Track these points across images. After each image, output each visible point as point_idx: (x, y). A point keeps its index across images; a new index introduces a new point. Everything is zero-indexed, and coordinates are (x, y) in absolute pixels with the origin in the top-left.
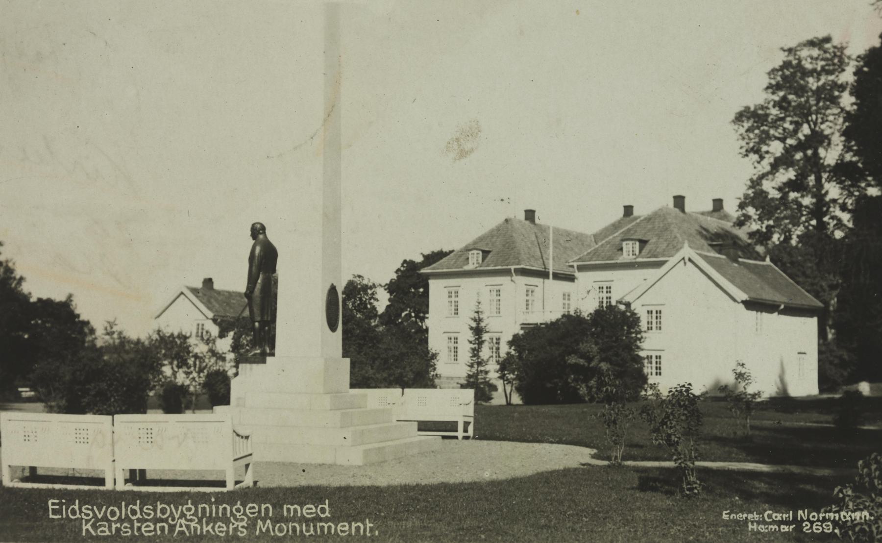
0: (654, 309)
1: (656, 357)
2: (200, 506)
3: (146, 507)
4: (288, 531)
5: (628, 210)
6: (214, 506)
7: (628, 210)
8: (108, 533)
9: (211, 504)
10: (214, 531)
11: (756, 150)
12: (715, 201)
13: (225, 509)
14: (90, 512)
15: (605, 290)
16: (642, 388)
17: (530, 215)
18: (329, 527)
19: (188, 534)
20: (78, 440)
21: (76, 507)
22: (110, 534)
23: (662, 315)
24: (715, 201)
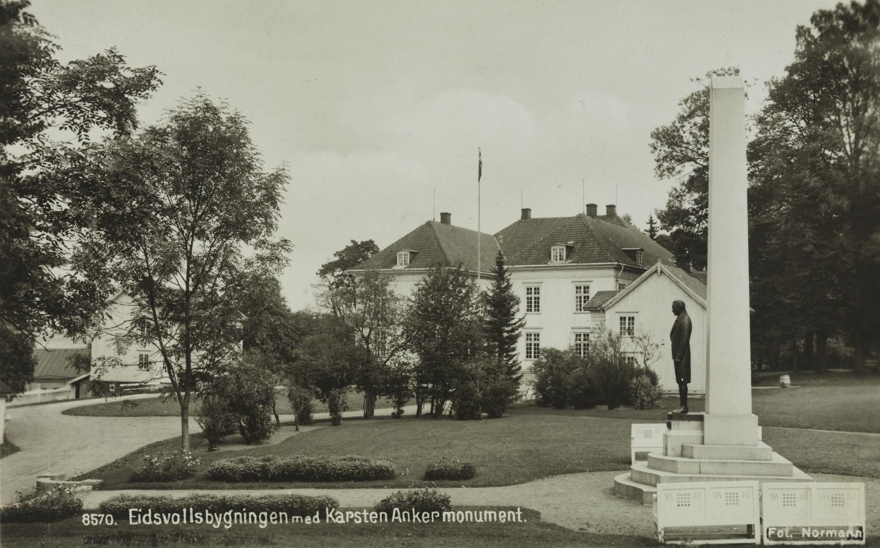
0: (627, 316)
1: (629, 318)
2: (433, 513)
3: (285, 514)
4: (223, 517)
5: (526, 212)
6: (245, 514)
7: (526, 212)
8: (342, 521)
9: (242, 513)
10: (421, 519)
11: (154, 88)
12: (608, 207)
13: (469, 514)
14: (360, 518)
15: (533, 291)
16: (202, 340)
17: (445, 217)
18: (493, 515)
19: (400, 521)
20: (687, 496)
21: (150, 515)
22: (482, 521)
23: (540, 300)
24: (608, 207)
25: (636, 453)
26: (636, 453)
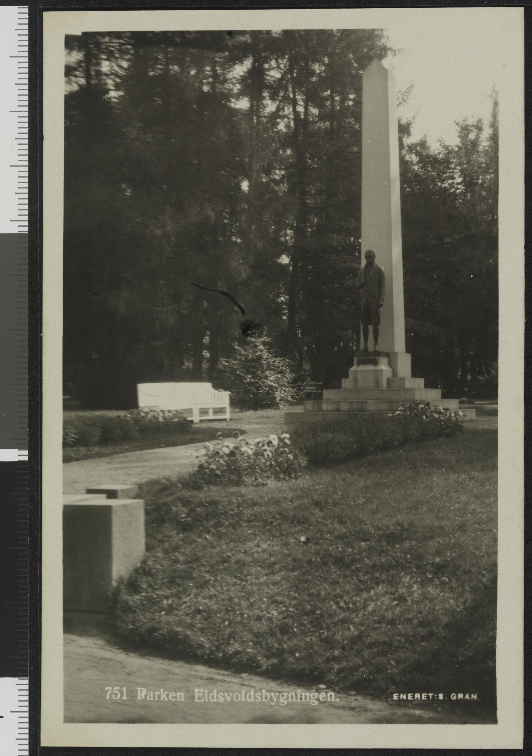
25: (68, 719)
26: (68, 719)
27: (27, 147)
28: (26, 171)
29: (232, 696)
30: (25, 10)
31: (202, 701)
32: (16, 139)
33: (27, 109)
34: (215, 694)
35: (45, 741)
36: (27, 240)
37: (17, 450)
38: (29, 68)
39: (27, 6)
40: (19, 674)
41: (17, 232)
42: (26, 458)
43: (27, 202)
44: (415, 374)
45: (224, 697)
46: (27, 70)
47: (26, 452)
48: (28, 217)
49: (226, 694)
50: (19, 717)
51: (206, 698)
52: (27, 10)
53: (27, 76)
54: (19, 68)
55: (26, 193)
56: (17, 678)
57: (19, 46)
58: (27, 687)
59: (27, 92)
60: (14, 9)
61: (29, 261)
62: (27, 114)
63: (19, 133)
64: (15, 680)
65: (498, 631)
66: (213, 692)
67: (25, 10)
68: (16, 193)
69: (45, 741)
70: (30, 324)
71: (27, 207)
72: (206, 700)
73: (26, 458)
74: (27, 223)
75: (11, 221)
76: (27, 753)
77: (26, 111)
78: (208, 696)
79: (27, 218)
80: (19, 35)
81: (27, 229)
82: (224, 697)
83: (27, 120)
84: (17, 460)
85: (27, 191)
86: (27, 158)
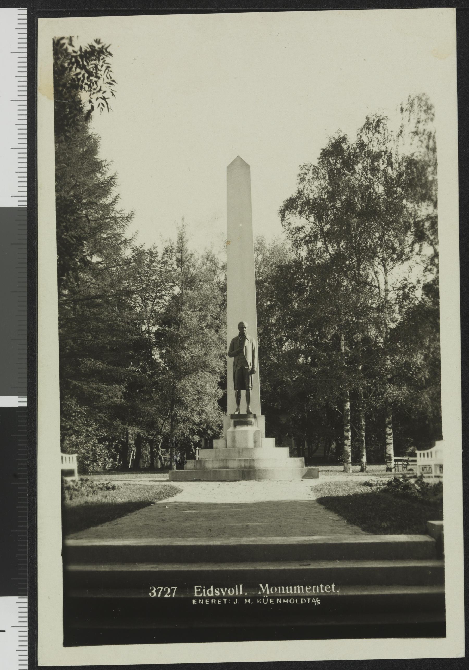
25: (68, 642)
26: (68, 642)
27: (26, 132)
28: (25, 29)
29: (227, 591)
30: (24, 11)
31: (201, 595)
32: (16, 77)
33: (26, 122)
34: (212, 589)
35: (41, 662)
36: (26, 213)
37: (17, 397)
38: (28, 148)
39: (26, 9)
40: (19, 593)
41: (17, 206)
42: (25, 405)
43: (26, 179)
44: (363, 455)
45: (220, 591)
46: (26, 65)
47: (25, 399)
48: (26, 59)
49: (222, 590)
50: (19, 655)
51: (204, 593)
52: (26, 12)
53: (26, 69)
54: (19, 665)
55: (25, 187)
56: (17, 597)
57: (18, 91)
58: (26, 605)
59: (26, 84)
60: (14, 11)
61: (28, 232)
62: (26, 103)
63: (19, 120)
64: (16, 599)
65: (440, 306)
66: (210, 588)
67: (24, 11)
68: (16, 172)
69: (41, 662)
70: (29, 287)
71: (26, 184)
72: (205, 595)
73: (25, 405)
74: (26, 199)
75: (11, 101)
76: (26, 667)
77: (25, 86)
78: (206, 592)
79: (26, 194)
80: (19, 607)
81: (26, 203)
82: (220, 591)
83: (26, 108)
84: (17, 406)
85: (26, 170)
86: (26, 141)
